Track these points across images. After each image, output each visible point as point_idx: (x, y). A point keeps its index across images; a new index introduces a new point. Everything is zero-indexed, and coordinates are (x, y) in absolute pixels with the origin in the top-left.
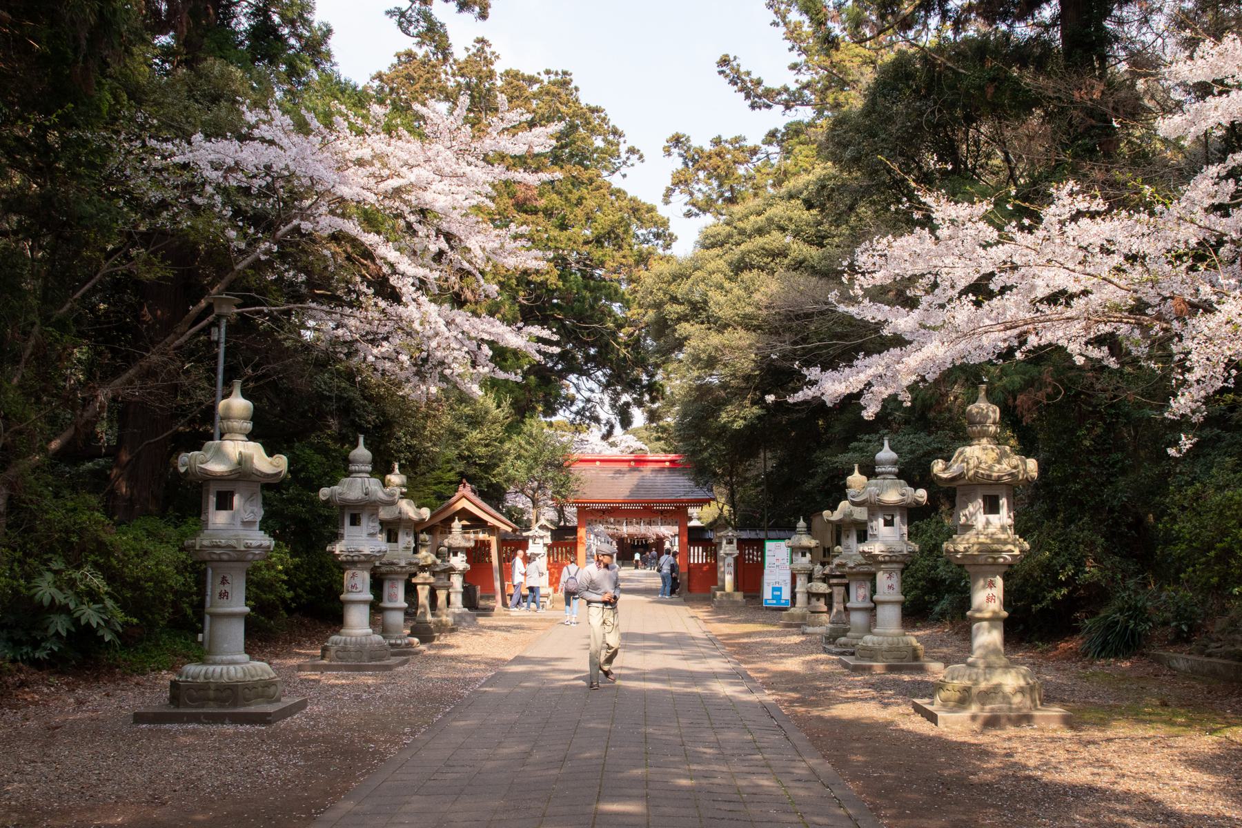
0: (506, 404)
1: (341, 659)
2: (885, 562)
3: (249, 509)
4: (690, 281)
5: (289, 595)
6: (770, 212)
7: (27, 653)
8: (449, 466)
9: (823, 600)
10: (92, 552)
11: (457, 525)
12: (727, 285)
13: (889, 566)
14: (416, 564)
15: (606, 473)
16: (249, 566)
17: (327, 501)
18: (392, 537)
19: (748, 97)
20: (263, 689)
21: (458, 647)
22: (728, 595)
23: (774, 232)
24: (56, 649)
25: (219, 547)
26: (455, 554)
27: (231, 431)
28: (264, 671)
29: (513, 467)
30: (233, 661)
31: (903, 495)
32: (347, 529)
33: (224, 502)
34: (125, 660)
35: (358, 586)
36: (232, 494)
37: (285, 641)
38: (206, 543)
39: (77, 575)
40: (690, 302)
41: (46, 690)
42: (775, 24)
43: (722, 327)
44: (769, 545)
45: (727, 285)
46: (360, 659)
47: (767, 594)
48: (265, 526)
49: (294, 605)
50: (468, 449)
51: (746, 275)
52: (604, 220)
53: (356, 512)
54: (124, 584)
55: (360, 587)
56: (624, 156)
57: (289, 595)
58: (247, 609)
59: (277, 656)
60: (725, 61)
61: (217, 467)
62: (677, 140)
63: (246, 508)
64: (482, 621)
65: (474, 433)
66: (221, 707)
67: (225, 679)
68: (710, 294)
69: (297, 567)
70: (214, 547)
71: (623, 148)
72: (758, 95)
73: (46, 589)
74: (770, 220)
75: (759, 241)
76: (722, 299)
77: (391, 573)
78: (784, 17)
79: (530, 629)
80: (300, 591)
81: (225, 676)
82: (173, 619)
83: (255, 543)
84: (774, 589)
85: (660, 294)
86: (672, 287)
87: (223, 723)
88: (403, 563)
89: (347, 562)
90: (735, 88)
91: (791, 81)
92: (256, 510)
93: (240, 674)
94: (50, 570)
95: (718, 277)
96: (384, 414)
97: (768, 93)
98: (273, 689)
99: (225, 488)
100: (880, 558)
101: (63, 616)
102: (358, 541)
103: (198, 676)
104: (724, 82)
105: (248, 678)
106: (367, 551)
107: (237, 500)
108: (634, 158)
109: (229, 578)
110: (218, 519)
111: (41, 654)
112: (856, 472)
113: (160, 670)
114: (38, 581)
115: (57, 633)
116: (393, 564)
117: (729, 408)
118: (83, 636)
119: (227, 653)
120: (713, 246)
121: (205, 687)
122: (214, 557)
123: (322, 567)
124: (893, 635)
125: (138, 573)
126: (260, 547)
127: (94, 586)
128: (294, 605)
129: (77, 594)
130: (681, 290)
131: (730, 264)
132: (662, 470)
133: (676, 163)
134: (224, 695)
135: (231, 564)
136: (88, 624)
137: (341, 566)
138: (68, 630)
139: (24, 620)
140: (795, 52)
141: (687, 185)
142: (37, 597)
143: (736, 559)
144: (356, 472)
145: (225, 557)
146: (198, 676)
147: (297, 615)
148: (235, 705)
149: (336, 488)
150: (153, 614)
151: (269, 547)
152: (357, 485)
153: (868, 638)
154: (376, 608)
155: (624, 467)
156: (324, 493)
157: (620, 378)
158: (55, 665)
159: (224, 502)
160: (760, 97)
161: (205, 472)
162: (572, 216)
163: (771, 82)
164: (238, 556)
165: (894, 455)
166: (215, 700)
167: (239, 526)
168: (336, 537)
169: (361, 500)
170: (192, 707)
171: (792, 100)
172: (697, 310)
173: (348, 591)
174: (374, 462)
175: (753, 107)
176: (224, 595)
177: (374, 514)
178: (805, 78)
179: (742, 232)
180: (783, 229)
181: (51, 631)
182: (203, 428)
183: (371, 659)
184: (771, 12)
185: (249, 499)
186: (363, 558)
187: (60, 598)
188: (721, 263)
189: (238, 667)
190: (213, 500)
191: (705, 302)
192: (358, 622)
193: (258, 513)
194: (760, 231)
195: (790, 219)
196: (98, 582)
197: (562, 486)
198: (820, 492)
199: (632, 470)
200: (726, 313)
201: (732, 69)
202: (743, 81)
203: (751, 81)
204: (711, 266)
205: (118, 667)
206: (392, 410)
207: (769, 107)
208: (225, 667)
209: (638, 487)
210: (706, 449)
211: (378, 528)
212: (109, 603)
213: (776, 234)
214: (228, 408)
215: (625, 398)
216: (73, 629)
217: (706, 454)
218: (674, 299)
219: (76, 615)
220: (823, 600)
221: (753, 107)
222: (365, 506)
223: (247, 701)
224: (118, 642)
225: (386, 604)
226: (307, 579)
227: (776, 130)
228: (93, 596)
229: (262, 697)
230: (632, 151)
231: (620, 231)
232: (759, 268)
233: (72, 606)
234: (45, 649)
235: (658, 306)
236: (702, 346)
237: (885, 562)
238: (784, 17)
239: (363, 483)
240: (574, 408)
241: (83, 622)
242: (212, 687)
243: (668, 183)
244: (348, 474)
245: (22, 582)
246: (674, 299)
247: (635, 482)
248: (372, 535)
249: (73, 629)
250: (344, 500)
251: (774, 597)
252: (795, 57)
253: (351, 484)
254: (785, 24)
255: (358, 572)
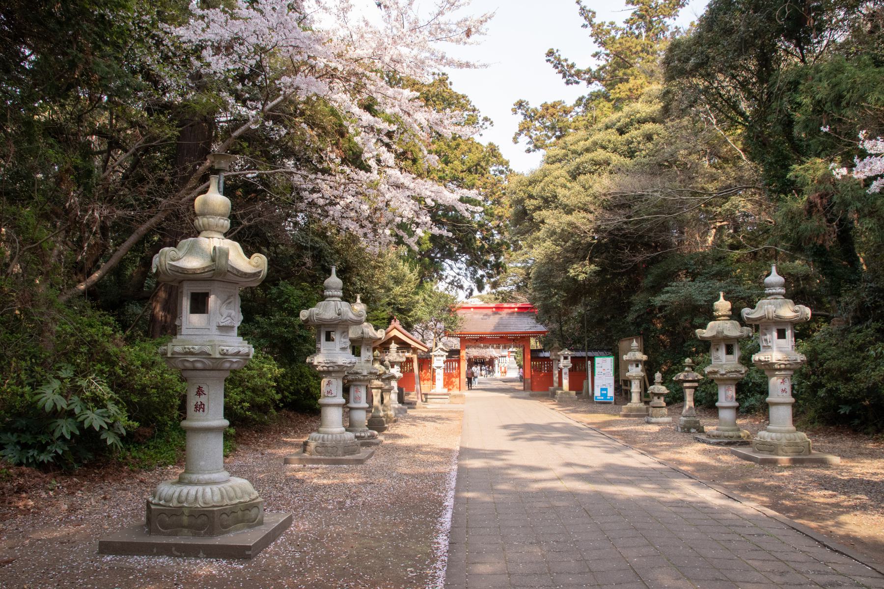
0: (416, 272)
1: (320, 453)
2: (780, 370)
3: (225, 311)
4: (542, 184)
5: (278, 397)
6: (594, 138)
7: (33, 456)
8: (383, 309)
9: (662, 398)
10: (100, 361)
11: (393, 346)
12: (568, 185)
13: (783, 373)
14: (375, 373)
15: (478, 316)
16: (228, 375)
17: (307, 321)
18: (356, 352)
19: (564, 77)
20: (243, 514)
21: (406, 437)
22: (566, 393)
23: (599, 150)
24: (60, 452)
25: (192, 354)
26: (393, 367)
27: (208, 228)
28: (244, 492)
29: (420, 311)
30: (214, 477)
31: (796, 311)
32: (323, 345)
33: (199, 304)
34: (134, 458)
35: (331, 391)
36: (206, 295)
37: (276, 432)
38: (178, 349)
39: (84, 383)
40: (542, 197)
41: (44, 495)
42: (584, 26)
43: (569, 211)
44: (598, 360)
45: (568, 185)
46: (335, 456)
47: (597, 393)
48: (243, 333)
49: (281, 405)
50: (394, 298)
51: (582, 178)
52: (470, 159)
53: (329, 329)
54: (133, 390)
55: (334, 392)
56: (481, 123)
57: (278, 397)
58: (226, 423)
59: (269, 447)
60: (551, 53)
61: (193, 263)
62: (520, 104)
63: (224, 311)
64: (411, 412)
65: (398, 288)
66: (195, 535)
67: (200, 504)
68: (557, 191)
69: (284, 376)
70: (186, 353)
71: (480, 119)
72: (570, 74)
73: (50, 396)
74: (595, 143)
75: (589, 156)
76: (567, 192)
77: (356, 380)
78: (590, 21)
79: (448, 419)
80: (287, 394)
81: (200, 499)
82: (157, 426)
83: (232, 350)
84: (602, 389)
85: (522, 194)
86: (530, 188)
87: (197, 557)
88: (365, 373)
89: (324, 372)
90: (557, 70)
91: (594, 65)
92: (233, 313)
93: (217, 498)
94: (58, 378)
95: (562, 180)
96: (346, 261)
97: (578, 73)
98: (254, 512)
99: (200, 289)
100: (776, 366)
101: (70, 420)
102: (330, 354)
103: (170, 500)
104: (550, 66)
105: (226, 502)
106: (340, 362)
107: (212, 300)
108: (487, 124)
109: (205, 388)
110: (191, 321)
111: (45, 458)
112: (722, 298)
113: (166, 464)
114: (43, 388)
115: (62, 437)
116: (357, 373)
117: (575, 266)
118: (88, 438)
119: (203, 472)
120: (553, 163)
121: (176, 512)
122: (187, 364)
123: (302, 376)
124: (789, 432)
125: (146, 380)
126: (237, 354)
127: (98, 393)
128: (281, 405)
129: (82, 399)
130: (536, 190)
131: (568, 172)
132: (513, 313)
133: (519, 118)
134: (199, 521)
135: (207, 373)
136: (91, 427)
137: (318, 376)
138: (72, 434)
139: (30, 427)
140: (596, 44)
141: (529, 131)
142: (40, 404)
143: (570, 370)
144: (330, 296)
145: (199, 365)
146: (170, 500)
147: (284, 410)
148: (211, 533)
149: (314, 310)
150: (162, 416)
151: (248, 355)
152: (329, 309)
153: (762, 433)
154: (347, 410)
155: (489, 312)
156: (304, 314)
157: (475, 262)
158: (59, 467)
159: (199, 304)
160: (572, 76)
161: (183, 271)
162: (453, 156)
163: (581, 66)
164: (213, 365)
165: (781, 279)
166: (189, 527)
167: (214, 331)
168: (314, 351)
169: (335, 320)
170: (164, 534)
171: (593, 77)
172: (549, 202)
173: (325, 396)
174: (345, 290)
175: (568, 83)
176: (200, 407)
177: (345, 332)
178: (602, 63)
179: (574, 152)
180: (604, 148)
181: (57, 434)
182: (182, 227)
183: (345, 453)
184: (582, 18)
185: (227, 301)
186: (336, 368)
187: (62, 404)
188: (563, 172)
189: (215, 488)
190: (186, 304)
191: (556, 197)
192: (333, 419)
193: (237, 318)
194: (587, 150)
195: (609, 141)
196: (103, 389)
197: (452, 323)
198: (633, 324)
199: (495, 313)
200: (572, 201)
201: (555, 58)
202: (562, 66)
203: (568, 65)
204: (556, 173)
205: (126, 464)
206: (352, 260)
207: (577, 83)
208: (200, 488)
209: (499, 324)
210: (554, 296)
211: (349, 343)
212: (112, 408)
213: (600, 151)
214: (205, 203)
215: (480, 272)
216: (78, 433)
217: (554, 299)
218: (531, 197)
219: (80, 419)
220: (662, 398)
221: (568, 83)
222: (337, 324)
223: (225, 528)
224: (120, 444)
225: (352, 405)
226: (291, 385)
227: (583, 97)
228: (98, 402)
229: (242, 521)
230: (486, 119)
231: (483, 164)
232: (590, 173)
233: (77, 411)
234: (50, 452)
235: (520, 201)
236: (556, 224)
237: (780, 370)
238: (590, 21)
239: (336, 305)
240: (448, 281)
241: (86, 426)
242: (186, 512)
243: (517, 130)
244: (323, 298)
245: (27, 389)
246: (531, 197)
247: (497, 321)
248: (343, 349)
249: (78, 433)
250: (321, 320)
251: (602, 395)
252: (596, 48)
253: (326, 306)
254: (592, 26)
255: (333, 380)
